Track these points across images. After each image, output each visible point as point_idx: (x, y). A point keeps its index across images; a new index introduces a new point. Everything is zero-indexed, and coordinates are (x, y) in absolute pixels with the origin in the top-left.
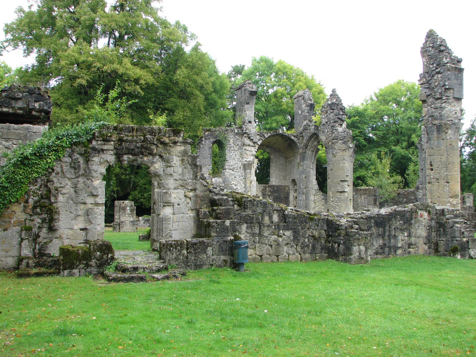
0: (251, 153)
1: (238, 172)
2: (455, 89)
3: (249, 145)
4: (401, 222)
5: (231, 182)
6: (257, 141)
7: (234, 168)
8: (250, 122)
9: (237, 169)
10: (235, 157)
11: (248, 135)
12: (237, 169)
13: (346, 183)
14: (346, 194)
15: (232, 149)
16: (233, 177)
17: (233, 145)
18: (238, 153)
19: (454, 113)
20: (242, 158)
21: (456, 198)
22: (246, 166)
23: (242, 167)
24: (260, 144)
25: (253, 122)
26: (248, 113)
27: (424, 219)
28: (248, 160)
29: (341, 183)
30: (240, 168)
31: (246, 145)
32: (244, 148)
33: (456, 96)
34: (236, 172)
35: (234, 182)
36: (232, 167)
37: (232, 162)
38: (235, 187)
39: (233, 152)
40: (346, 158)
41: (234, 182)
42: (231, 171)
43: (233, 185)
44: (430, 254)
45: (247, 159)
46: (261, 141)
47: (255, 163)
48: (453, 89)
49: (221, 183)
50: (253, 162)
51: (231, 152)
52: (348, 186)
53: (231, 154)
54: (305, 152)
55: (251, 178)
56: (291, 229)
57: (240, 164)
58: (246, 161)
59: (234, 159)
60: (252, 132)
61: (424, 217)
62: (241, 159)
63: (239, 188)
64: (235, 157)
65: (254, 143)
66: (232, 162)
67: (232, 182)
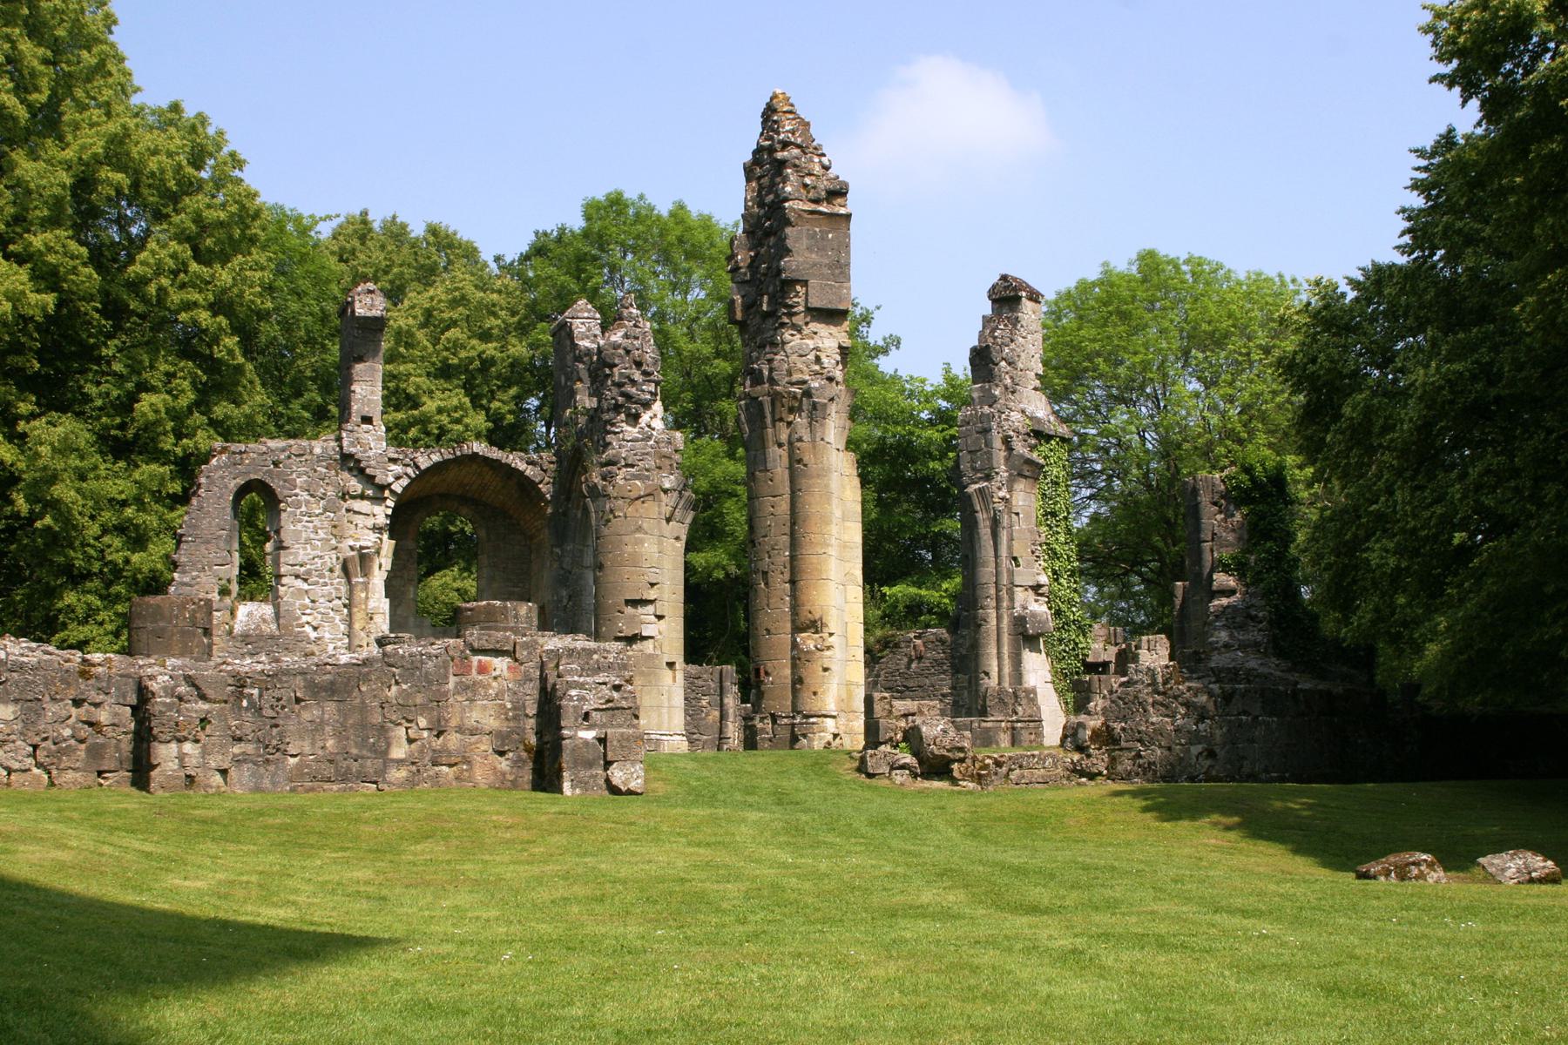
0: (370, 522)
1: (325, 584)
2: (811, 282)
3: (362, 497)
4: (404, 687)
5: (298, 618)
6: (391, 479)
7: (309, 572)
8: (367, 420)
9: (322, 576)
10: (312, 536)
11: (359, 461)
12: (322, 576)
13: (650, 609)
14: (648, 646)
15: (303, 509)
16: (307, 601)
17: (305, 496)
18: (322, 522)
19: (811, 357)
20: (341, 538)
21: (817, 632)
22: (355, 565)
23: (338, 568)
24: (399, 490)
25: (377, 420)
26: (358, 388)
27: (495, 678)
28: (358, 545)
29: (629, 610)
30: (331, 570)
31: (353, 497)
32: (346, 505)
33: (815, 302)
34: (316, 583)
35: (309, 619)
36: (303, 569)
37: (301, 552)
38: (313, 635)
39: (306, 518)
40: (645, 526)
41: (309, 619)
42: (299, 584)
43: (308, 629)
44: (515, 785)
45: (358, 540)
46: (405, 482)
47: (383, 552)
48: (807, 281)
49: (264, 621)
50: (378, 552)
51: (300, 521)
52: (660, 617)
53: (299, 526)
54: (565, 514)
55: (372, 604)
56: (16, 701)
57: (331, 559)
58: (352, 548)
59: (308, 541)
60: (371, 453)
61: (494, 674)
62: (333, 542)
63: (327, 635)
64: (312, 536)
65: (382, 488)
66: (301, 552)
67: (305, 619)
